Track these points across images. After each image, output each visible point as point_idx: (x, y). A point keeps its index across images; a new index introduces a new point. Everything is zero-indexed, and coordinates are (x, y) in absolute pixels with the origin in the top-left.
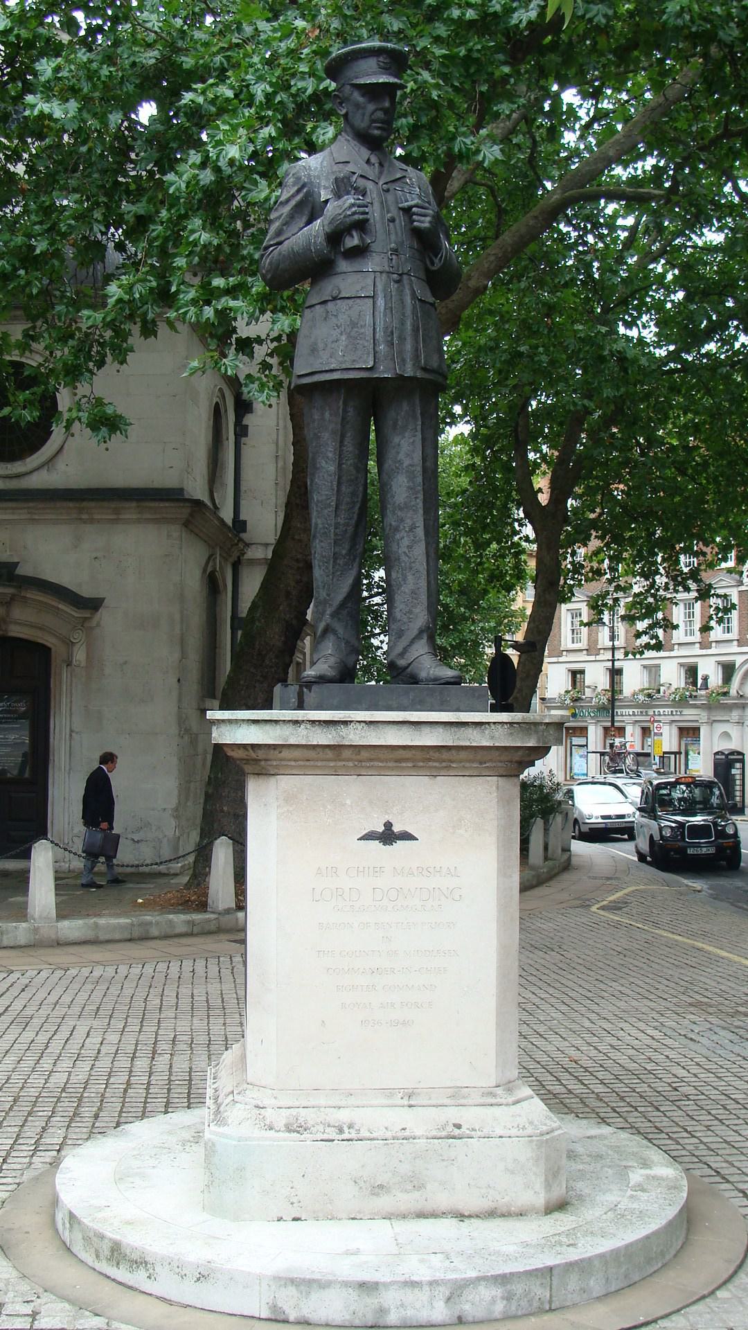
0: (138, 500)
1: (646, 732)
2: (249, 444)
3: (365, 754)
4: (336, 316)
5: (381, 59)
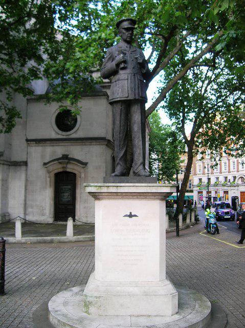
3: (124, 194)
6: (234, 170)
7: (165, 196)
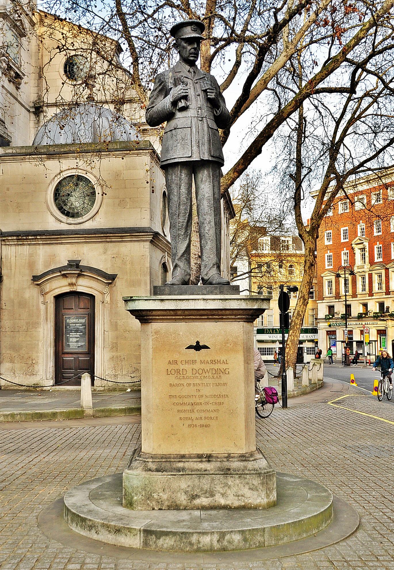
1: (362, 332)
5: (193, 27)
6: (364, 292)
7: (251, 315)
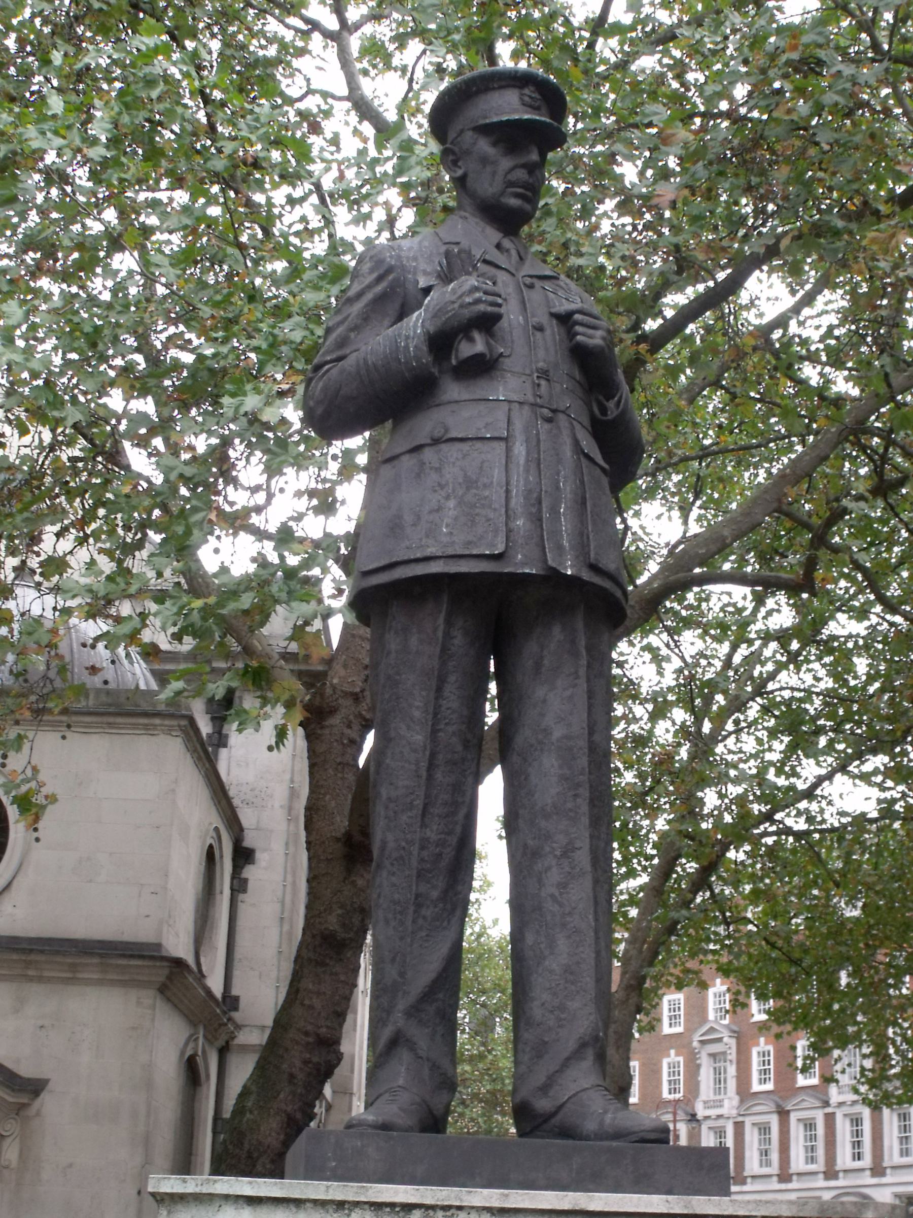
0: (101, 956)
2: (247, 901)
4: (438, 470)
5: (526, 91)
